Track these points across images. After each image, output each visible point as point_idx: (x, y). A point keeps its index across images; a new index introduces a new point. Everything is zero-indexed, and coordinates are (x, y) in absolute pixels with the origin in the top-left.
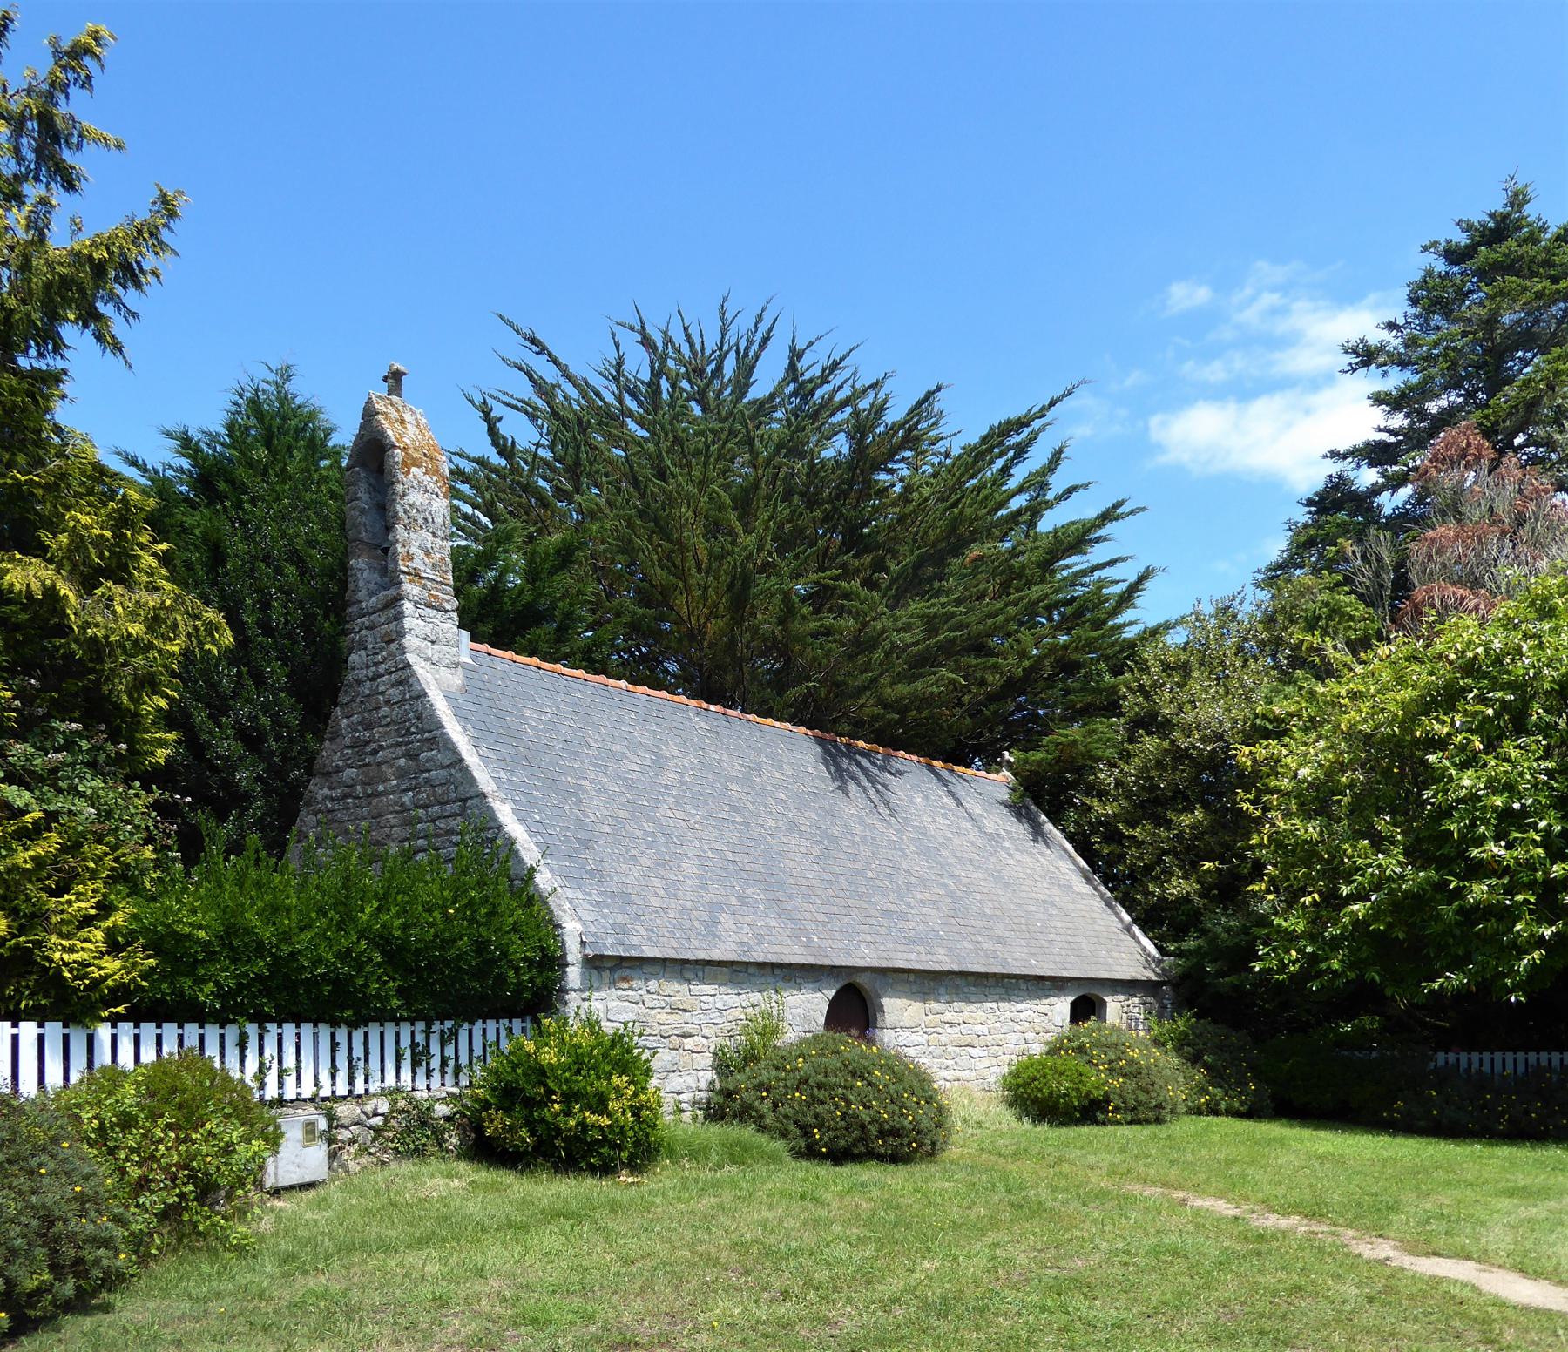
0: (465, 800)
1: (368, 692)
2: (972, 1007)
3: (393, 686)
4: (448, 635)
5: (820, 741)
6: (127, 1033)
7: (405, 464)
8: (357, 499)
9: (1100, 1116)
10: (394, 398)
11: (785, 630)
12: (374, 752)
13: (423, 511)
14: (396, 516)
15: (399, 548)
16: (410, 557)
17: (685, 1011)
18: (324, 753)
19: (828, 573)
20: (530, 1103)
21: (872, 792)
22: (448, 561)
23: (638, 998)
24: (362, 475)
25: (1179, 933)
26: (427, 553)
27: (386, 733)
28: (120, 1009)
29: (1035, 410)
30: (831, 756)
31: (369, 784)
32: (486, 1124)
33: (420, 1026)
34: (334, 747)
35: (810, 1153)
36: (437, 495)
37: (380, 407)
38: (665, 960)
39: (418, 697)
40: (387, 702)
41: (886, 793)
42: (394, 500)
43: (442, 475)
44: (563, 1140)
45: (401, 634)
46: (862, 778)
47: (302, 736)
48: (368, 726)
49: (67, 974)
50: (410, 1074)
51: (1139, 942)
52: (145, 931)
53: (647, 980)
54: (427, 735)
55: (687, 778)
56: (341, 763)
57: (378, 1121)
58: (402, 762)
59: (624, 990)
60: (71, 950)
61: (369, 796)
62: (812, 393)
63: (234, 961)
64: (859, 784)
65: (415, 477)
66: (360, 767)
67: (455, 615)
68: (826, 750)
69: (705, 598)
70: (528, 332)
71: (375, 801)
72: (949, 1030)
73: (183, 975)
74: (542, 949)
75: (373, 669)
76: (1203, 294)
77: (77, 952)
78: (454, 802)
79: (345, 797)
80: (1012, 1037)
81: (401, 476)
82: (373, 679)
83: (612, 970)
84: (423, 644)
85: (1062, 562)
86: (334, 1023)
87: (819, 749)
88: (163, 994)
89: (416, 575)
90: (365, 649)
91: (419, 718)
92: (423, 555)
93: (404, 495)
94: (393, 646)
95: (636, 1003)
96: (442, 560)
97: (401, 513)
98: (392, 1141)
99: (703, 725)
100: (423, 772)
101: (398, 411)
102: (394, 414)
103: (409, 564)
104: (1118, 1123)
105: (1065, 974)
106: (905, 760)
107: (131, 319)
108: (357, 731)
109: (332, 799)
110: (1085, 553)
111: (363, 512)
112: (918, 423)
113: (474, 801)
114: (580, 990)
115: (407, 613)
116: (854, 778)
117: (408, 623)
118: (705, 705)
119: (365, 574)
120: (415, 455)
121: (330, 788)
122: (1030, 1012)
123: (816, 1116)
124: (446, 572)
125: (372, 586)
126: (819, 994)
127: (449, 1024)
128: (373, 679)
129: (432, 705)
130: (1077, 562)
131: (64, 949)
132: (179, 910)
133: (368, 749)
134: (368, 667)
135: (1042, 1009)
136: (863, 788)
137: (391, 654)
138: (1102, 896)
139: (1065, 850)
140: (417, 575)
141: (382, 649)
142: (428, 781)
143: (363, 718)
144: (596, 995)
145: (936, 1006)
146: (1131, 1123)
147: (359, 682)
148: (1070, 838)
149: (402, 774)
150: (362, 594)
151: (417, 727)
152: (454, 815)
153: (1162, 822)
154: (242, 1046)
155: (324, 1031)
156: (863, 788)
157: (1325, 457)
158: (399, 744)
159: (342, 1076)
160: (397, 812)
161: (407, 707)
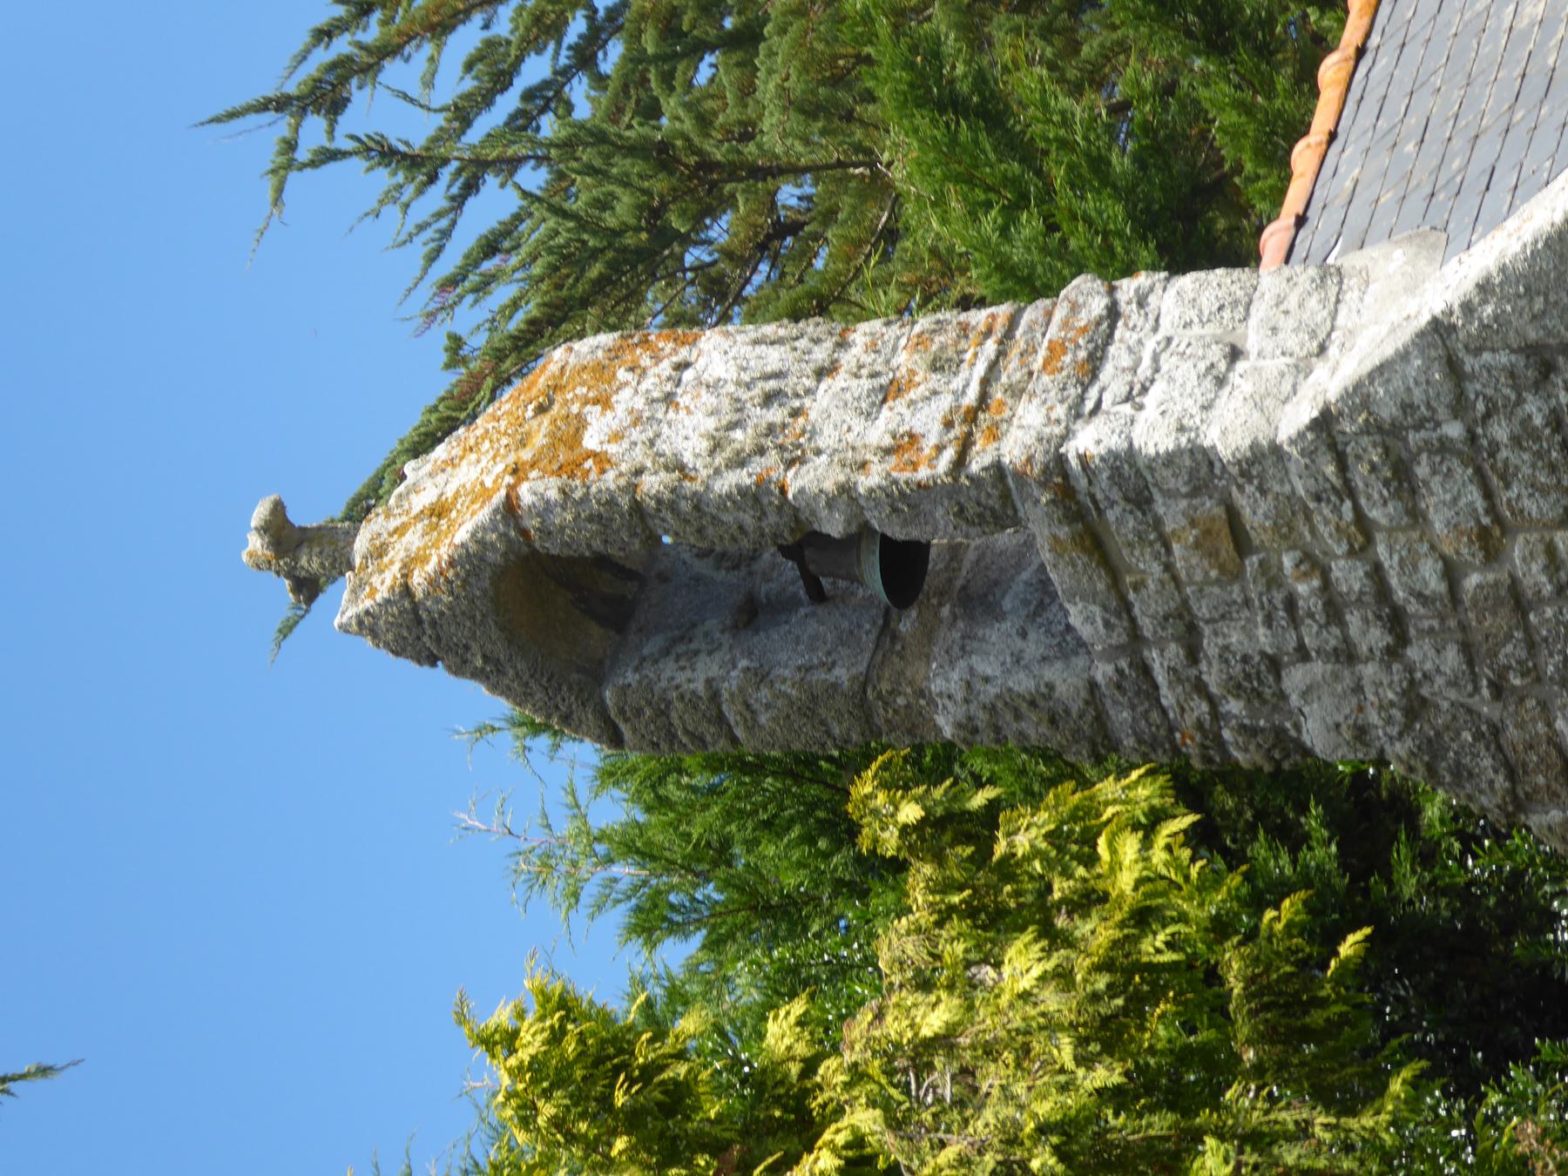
1: (1452, 658)
3: (1416, 516)
4: (1208, 302)
7: (571, 469)
8: (715, 696)
14: (753, 497)
15: (867, 482)
16: (904, 444)
24: (631, 677)
26: (889, 392)
36: (682, 366)
37: (384, 583)
39: (1453, 367)
40: (1490, 543)
42: (698, 501)
43: (614, 353)
65: (617, 437)
67: (1128, 288)
75: (1354, 620)
81: (610, 480)
82: (1396, 622)
84: (1242, 379)
90: (1275, 665)
92: (900, 405)
93: (681, 467)
94: (1255, 512)
96: (921, 342)
97: (742, 477)
111: (761, 676)
115: (1116, 442)
119: (985, 667)
120: (540, 440)
124: (964, 329)
125: (1033, 647)
128: (1396, 622)
129: (1484, 288)
134: (1347, 655)
137: (1289, 517)
141: (1272, 578)
147: (1415, 706)
150: (1065, 681)
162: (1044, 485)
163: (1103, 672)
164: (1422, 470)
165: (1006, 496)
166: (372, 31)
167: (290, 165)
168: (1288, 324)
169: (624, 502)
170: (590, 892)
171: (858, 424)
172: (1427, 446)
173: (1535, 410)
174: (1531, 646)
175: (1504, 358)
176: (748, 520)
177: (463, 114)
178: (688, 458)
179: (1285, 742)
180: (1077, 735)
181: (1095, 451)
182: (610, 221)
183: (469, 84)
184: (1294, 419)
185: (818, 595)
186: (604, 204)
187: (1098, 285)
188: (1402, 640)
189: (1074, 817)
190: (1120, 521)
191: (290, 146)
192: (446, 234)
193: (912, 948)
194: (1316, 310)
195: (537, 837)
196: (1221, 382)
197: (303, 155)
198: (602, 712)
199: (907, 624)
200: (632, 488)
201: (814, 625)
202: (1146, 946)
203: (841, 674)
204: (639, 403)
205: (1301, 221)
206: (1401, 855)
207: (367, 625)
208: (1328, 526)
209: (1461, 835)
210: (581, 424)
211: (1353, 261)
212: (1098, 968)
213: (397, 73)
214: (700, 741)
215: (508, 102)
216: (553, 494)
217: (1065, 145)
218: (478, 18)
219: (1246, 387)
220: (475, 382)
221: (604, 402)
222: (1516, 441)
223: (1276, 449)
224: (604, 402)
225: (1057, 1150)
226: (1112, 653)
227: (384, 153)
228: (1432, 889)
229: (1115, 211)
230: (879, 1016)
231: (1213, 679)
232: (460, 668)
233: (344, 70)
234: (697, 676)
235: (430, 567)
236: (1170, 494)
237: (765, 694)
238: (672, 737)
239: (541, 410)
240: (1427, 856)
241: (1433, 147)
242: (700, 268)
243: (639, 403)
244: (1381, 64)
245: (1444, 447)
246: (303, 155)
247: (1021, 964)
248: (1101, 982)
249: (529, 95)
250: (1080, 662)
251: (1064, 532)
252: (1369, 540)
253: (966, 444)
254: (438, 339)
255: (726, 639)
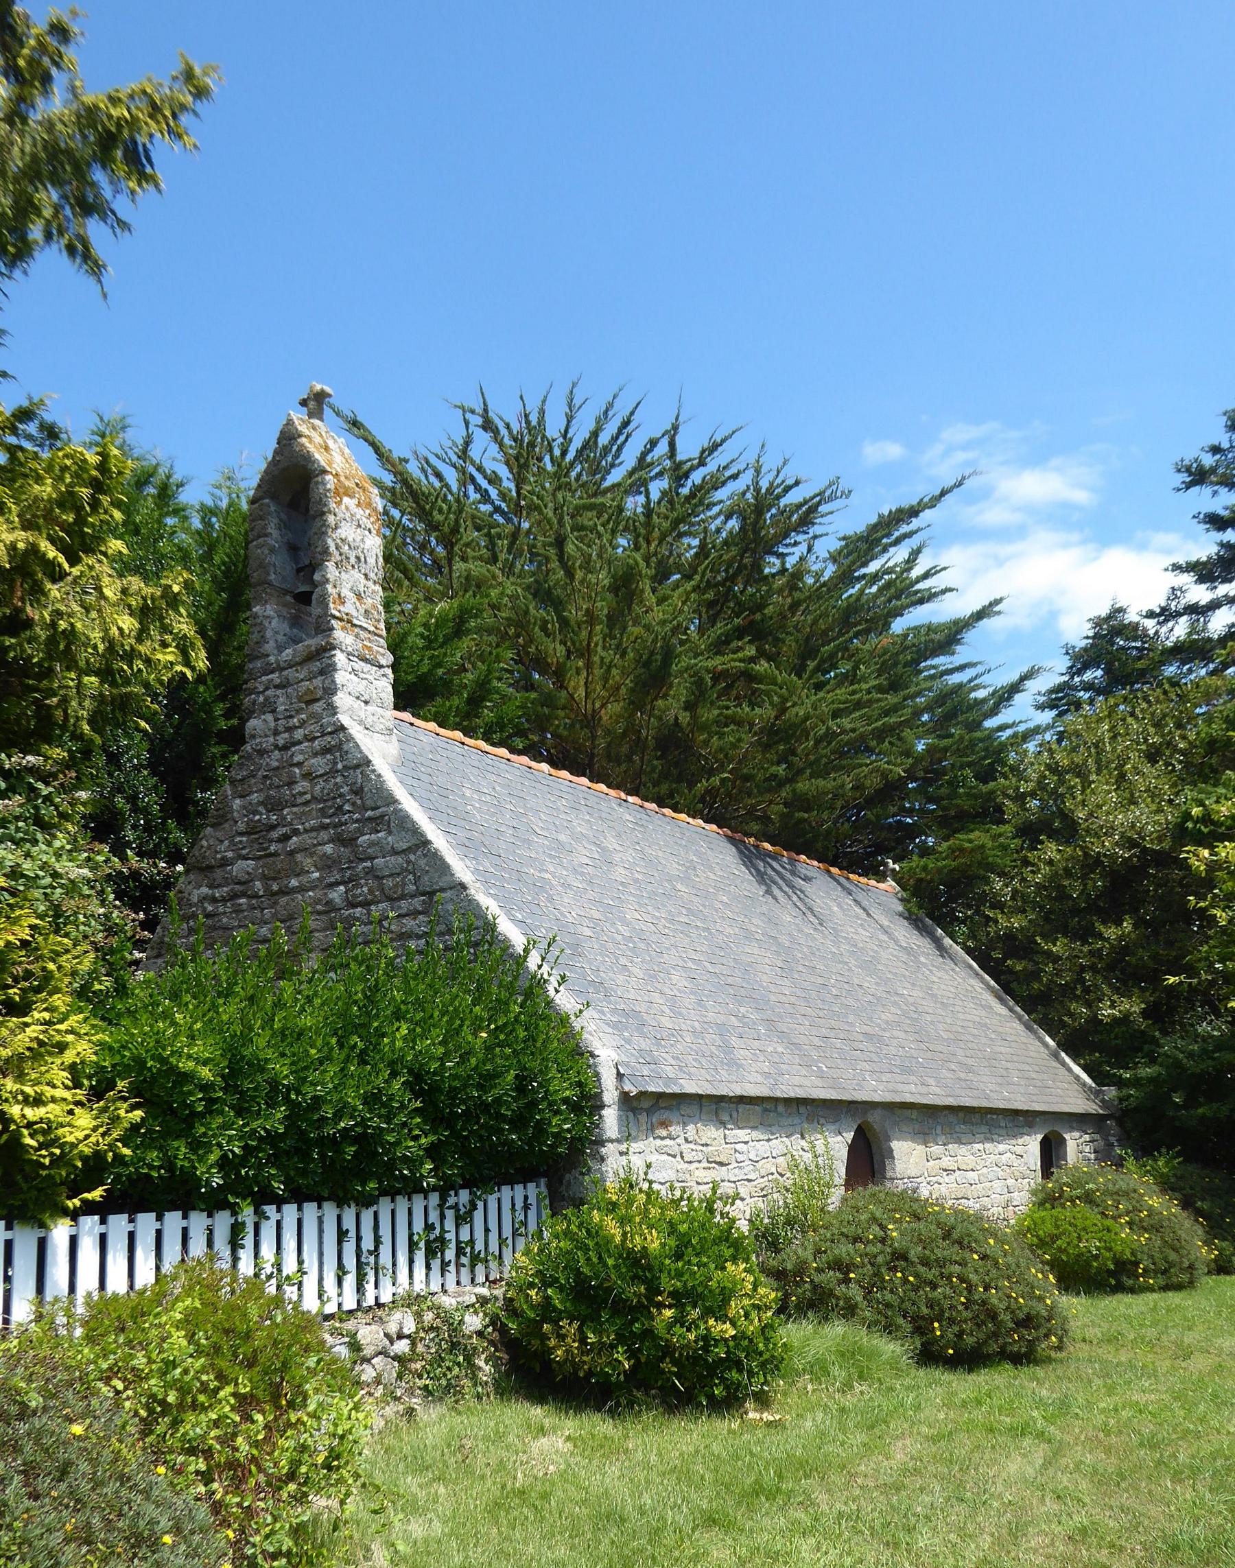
0: (431, 894)
1: (276, 764)
2: (963, 1150)
3: (315, 755)
4: (382, 695)
5: (731, 840)
6: (90, 1232)
7: (337, 493)
8: (266, 535)
9: (1129, 1282)
10: (316, 422)
11: (694, 717)
12: (285, 838)
13: (356, 548)
14: (326, 551)
15: (329, 587)
17: (721, 1164)
18: (204, 843)
19: (740, 655)
20: (622, 1308)
21: (795, 898)
22: (381, 608)
23: (676, 1150)
24: (273, 509)
25: (1122, 1057)
26: (359, 596)
27: (303, 813)
28: (96, 1194)
29: (926, 500)
30: (749, 857)
31: (274, 879)
32: (552, 1343)
33: (434, 1198)
34: (219, 834)
35: (929, 1356)
36: (370, 531)
37: (303, 429)
38: (700, 1097)
39: (358, 766)
40: (308, 776)
41: (807, 900)
42: (325, 533)
43: (375, 510)
44: (675, 1362)
45: (331, 690)
46: (780, 882)
47: (164, 823)
48: (274, 806)
49: (28, 1141)
50: (424, 1271)
51: (1070, 1070)
52: (121, 1070)
53: (685, 1124)
54: (369, 813)
55: (637, 875)
56: (230, 854)
57: (402, 1347)
58: (329, 849)
59: (662, 1138)
60: (38, 1101)
61: (274, 894)
62: (686, 475)
63: (240, 1112)
64: (780, 888)
65: (347, 508)
66: (260, 858)
67: (389, 671)
68: (740, 852)
69: (605, 679)
70: (350, 414)
71: (283, 900)
72: (947, 1179)
73: (177, 1137)
74: (580, 1084)
75: (286, 735)
76: (894, 450)
77: (44, 1104)
78: (412, 896)
79: (234, 896)
80: (997, 1185)
81: (333, 505)
82: (285, 748)
83: (650, 1111)
85: (929, 663)
86: (341, 1203)
87: (734, 849)
88: (151, 1167)
89: (349, 621)
90: (273, 711)
91: (358, 792)
94: (318, 707)
95: (674, 1156)
97: (332, 548)
98: (420, 1377)
99: (628, 817)
100: (363, 860)
101: (321, 436)
102: (318, 440)
103: (341, 608)
104: (1151, 1289)
105: (1037, 1107)
106: (808, 865)
107: (118, 230)
108: (255, 812)
109: (214, 900)
110: (953, 654)
111: (272, 550)
112: (819, 504)
113: (448, 894)
114: (618, 1141)
115: (339, 666)
116: (775, 883)
117: (341, 677)
118: (623, 795)
119: (274, 623)
120: (347, 483)
121: (211, 887)
122: (1009, 1154)
123: (931, 1304)
124: (379, 621)
125: (280, 638)
126: (839, 1138)
127: (464, 1196)
128: (285, 748)
129: (379, 776)
130: (942, 661)
131: (27, 1101)
132: (176, 1035)
133: (275, 834)
134: (276, 733)
135: (1019, 1150)
136: (785, 892)
137: (316, 717)
138: (1020, 1018)
139: (971, 967)
140: (349, 622)
141: (298, 711)
142: (370, 872)
143: (268, 797)
144: (635, 1146)
145: (936, 1149)
146: (1166, 1288)
147: (261, 753)
148: (968, 951)
149: (327, 864)
150: (269, 647)
151: (354, 804)
152: (414, 914)
153: (1085, 934)
154: (235, 1244)
155: (330, 1210)
156: (785, 892)
157: (1166, 570)
158: (324, 827)
159: (350, 1281)
160: (319, 913)
161: (339, 779)
162: (327, 643)
163: (272, 659)
164: (328, 756)
165: (324, 631)
166: (508, 441)
167: (464, 411)
168: (375, 719)
169: (325, 509)
170: (217, 492)
171: (349, 586)
172: (335, 758)
173: (345, 789)
174: (278, 787)
175: (359, 781)
176: (319, 549)
177: (480, 469)
178: (339, 531)
179: (251, 714)
180: (253, 650)
181: (336, 659)
182: (435, 513)
183: (489, 472)
184: (344, 719)
185: (299, 571)
186: (440, 511)
187: (390, 663)
188: (280, 749)
189: (192, 643)
190: (316, 666)
191: (473, 412)
192: (444, 461)
193: (134, 588)
194: (379, 727)
195: (238, 476)
196: (358, 698)
197: (468, 415)
198: (261, 498)
199: (289, 598)
200: (330, 512)
201: (289, 569)
202: (139, 662)
203: (272, 577)
204: (358, 516)
205: (412, 724)
206: (225, 748)
207: (290, 422)
208: (312, 728)
209: (230, 766)
210: (352, 497)
211: (394, 738)
212: (132, 646)
213: (494, 448)
214: (252, 529)
215: (484, 484)
216: (328, 486)
217: (445, 654)
218: (510, 476)
219: (356, 706)
220: (393, 465)
221: (359, 505)
222: (336, 784)
223: (336, 713)
224: (359, 505)
225: (66, 629)
226: (277, 661)
227: (467, 443)
228: (214, 756)
229: (425, 668)
230: (110, 576)
231: (269, 693)
232: (276, 452)
233: (496, 432)
234: (272, 529)
235: (307, 445)
236: (323, 681)
237: (267, 552)
238: (253, 521)
239: (357, 485)
240: (224, 756)
241: (429, 763)
242: (429, 542)
243: (358, 516)
244: (458, 749)
245: (335, 763)
246: (468, 415)
247: (128, 623)
248: (127, 648)
249: (486, 491)
250: (276, 652)
251: (313, 649)
252: (309, 741)
253: (341, 620)
254: (408, 454)
255: (285, 540)
